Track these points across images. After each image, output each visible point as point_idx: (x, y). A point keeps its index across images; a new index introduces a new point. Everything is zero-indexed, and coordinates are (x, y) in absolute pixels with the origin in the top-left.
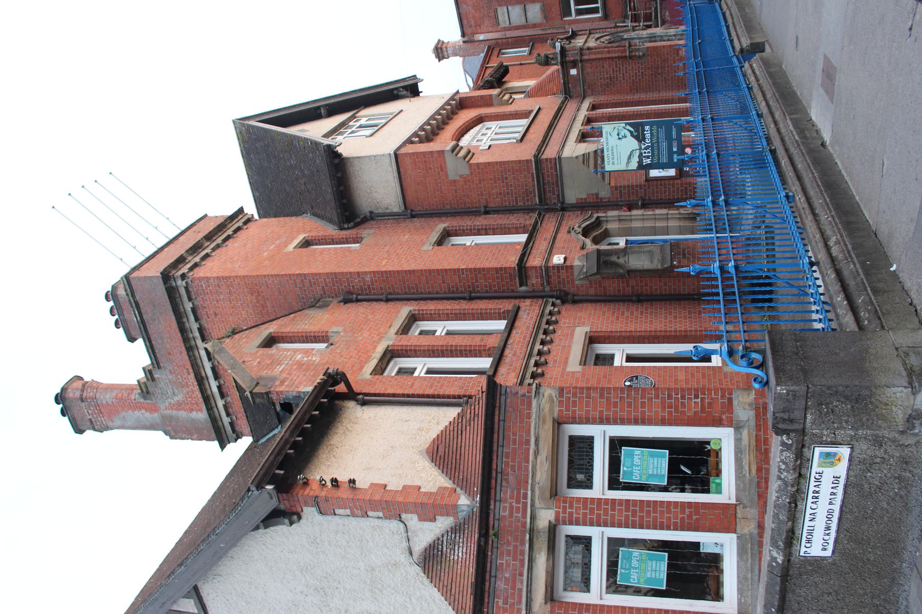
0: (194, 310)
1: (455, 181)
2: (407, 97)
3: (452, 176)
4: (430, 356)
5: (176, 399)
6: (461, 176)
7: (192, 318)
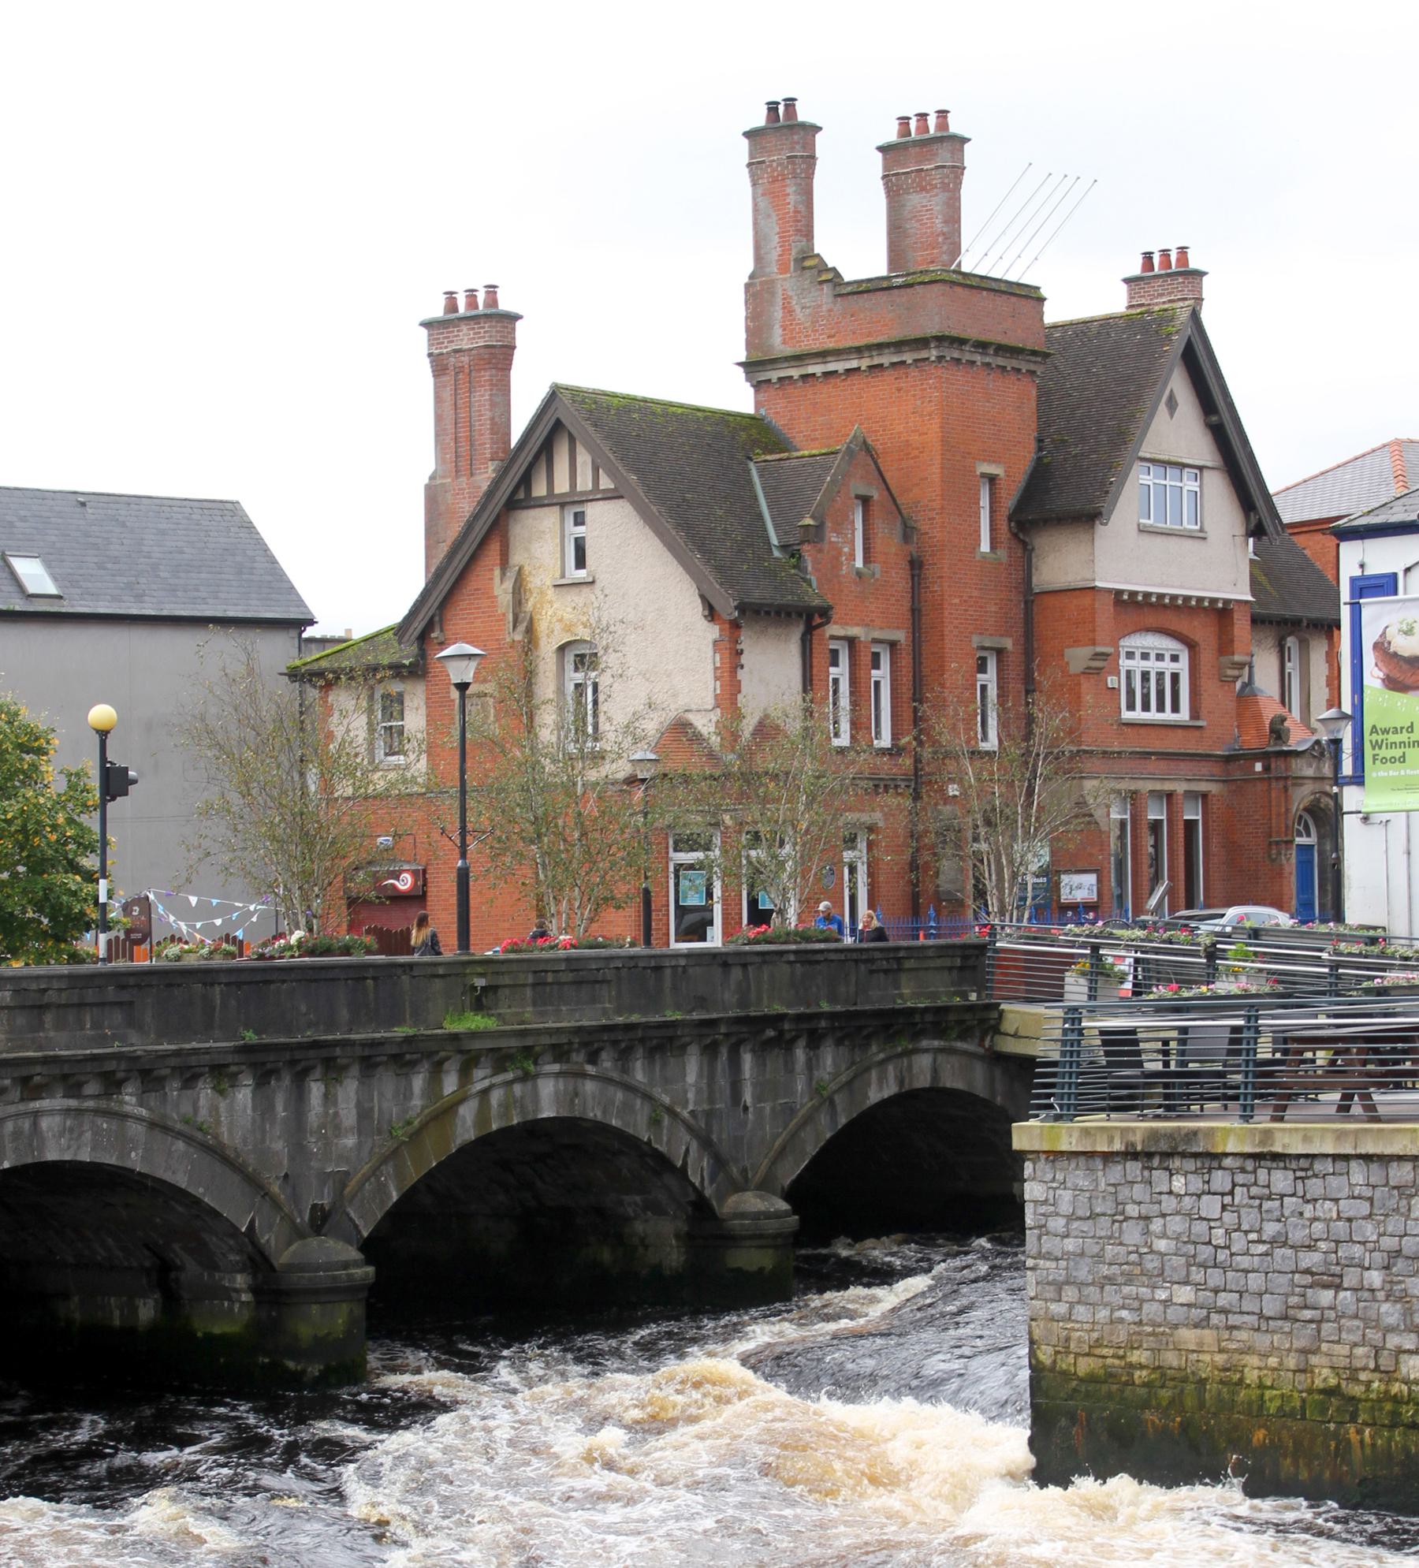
1: (1063, 655)
2: (1247, 524)
4: (850, 679)
5: (798, 310)
6: (1067, 663)
7: (895, 359)
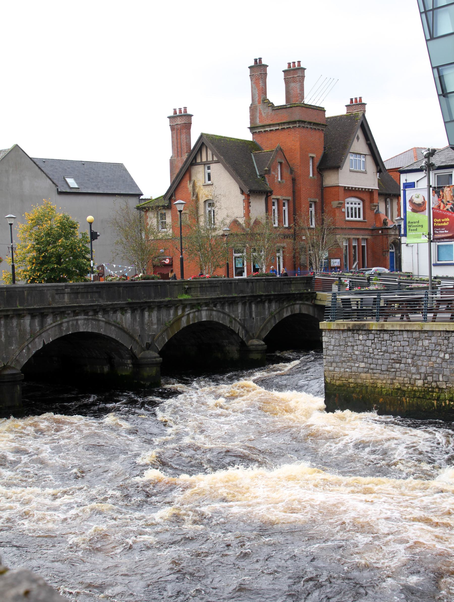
0: (290, 127)
3: (333, 203)
5: (263, 113)
7: (288, 127)
